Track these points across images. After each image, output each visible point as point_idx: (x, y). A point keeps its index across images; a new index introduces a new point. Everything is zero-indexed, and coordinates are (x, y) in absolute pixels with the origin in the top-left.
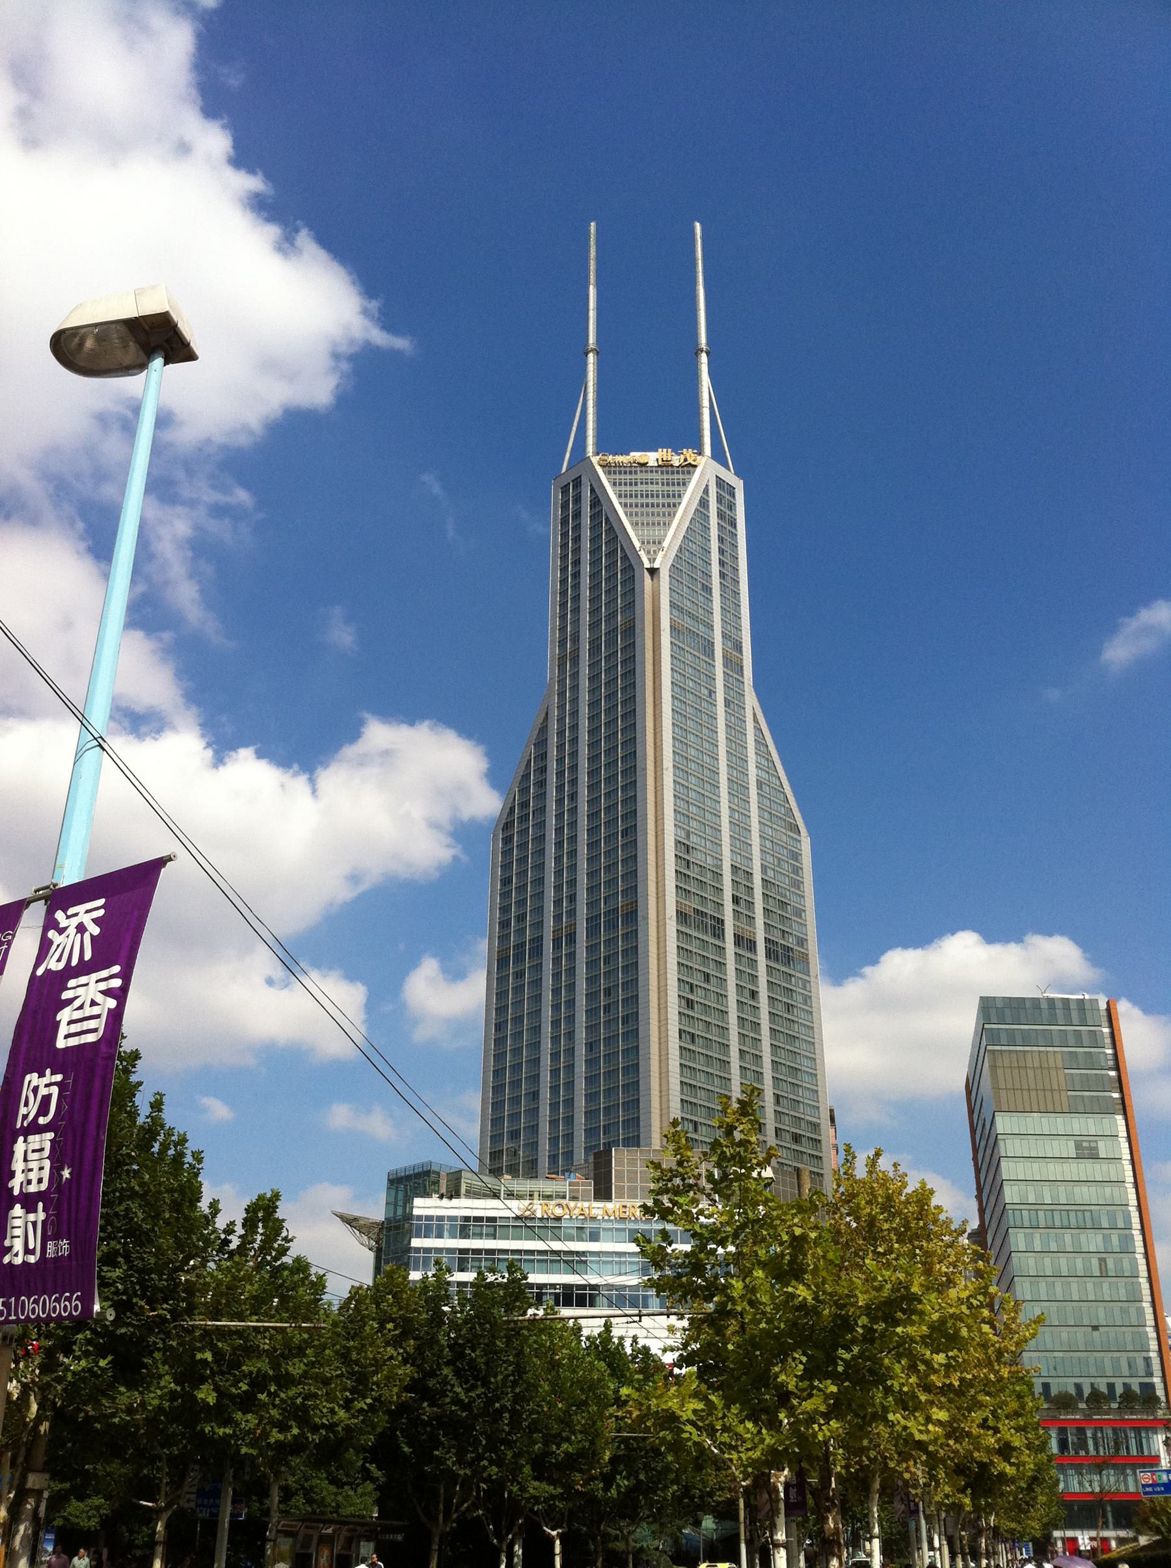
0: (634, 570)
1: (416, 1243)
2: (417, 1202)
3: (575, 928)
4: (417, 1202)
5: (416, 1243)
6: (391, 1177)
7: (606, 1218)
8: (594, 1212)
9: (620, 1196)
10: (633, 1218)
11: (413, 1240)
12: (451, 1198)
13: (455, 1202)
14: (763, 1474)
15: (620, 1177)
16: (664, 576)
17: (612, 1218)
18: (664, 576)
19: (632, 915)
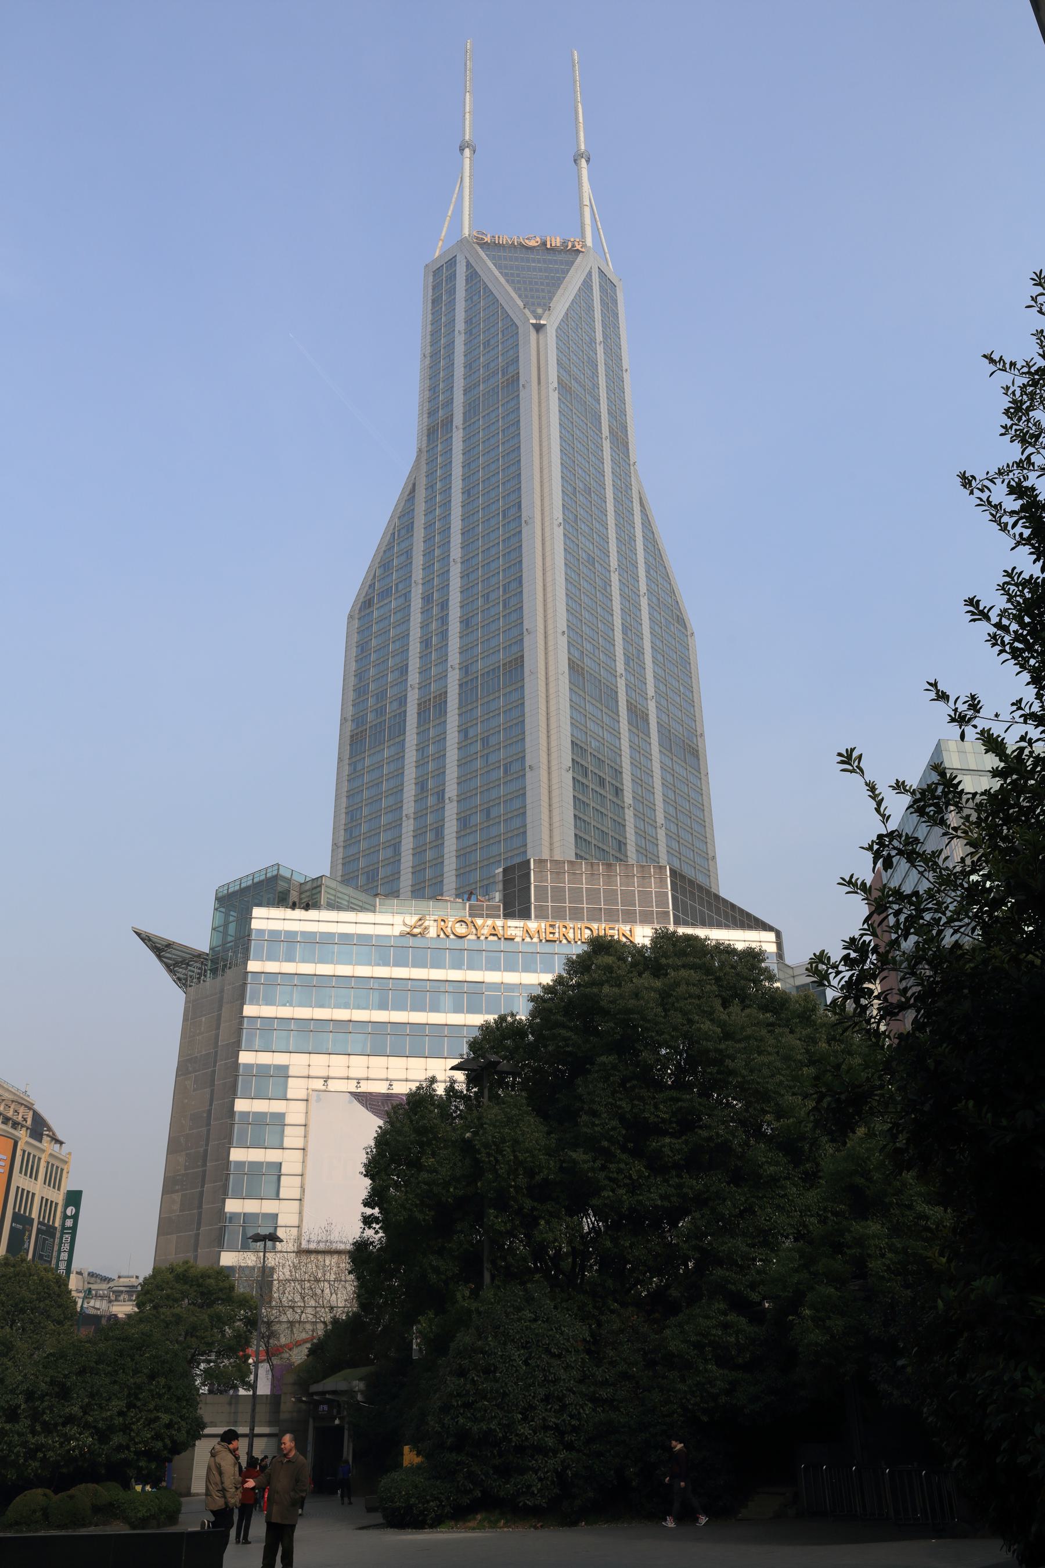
0: (517, 328)
1: (237, 1155)
2: (257, 912)
3: (446, 697)
4: (257, 912)
5: (232, 1206)
6: (220, 895)
7: (528, 939)
8: (510, 932)
9: (541, 915)
10: (564, 941)
11: (241, 1053)
12: (307, 907)
13: (313, 914)
14: (156, 1487)
15: (541, 891)
16: (551, 332)
17: (535, 940)
18: (551, 332)
19: (516, 666)
